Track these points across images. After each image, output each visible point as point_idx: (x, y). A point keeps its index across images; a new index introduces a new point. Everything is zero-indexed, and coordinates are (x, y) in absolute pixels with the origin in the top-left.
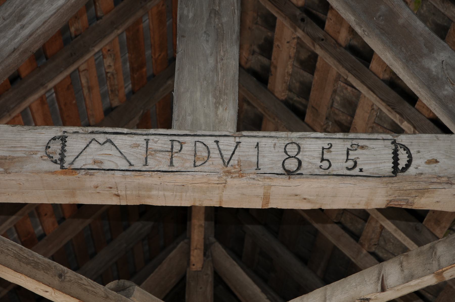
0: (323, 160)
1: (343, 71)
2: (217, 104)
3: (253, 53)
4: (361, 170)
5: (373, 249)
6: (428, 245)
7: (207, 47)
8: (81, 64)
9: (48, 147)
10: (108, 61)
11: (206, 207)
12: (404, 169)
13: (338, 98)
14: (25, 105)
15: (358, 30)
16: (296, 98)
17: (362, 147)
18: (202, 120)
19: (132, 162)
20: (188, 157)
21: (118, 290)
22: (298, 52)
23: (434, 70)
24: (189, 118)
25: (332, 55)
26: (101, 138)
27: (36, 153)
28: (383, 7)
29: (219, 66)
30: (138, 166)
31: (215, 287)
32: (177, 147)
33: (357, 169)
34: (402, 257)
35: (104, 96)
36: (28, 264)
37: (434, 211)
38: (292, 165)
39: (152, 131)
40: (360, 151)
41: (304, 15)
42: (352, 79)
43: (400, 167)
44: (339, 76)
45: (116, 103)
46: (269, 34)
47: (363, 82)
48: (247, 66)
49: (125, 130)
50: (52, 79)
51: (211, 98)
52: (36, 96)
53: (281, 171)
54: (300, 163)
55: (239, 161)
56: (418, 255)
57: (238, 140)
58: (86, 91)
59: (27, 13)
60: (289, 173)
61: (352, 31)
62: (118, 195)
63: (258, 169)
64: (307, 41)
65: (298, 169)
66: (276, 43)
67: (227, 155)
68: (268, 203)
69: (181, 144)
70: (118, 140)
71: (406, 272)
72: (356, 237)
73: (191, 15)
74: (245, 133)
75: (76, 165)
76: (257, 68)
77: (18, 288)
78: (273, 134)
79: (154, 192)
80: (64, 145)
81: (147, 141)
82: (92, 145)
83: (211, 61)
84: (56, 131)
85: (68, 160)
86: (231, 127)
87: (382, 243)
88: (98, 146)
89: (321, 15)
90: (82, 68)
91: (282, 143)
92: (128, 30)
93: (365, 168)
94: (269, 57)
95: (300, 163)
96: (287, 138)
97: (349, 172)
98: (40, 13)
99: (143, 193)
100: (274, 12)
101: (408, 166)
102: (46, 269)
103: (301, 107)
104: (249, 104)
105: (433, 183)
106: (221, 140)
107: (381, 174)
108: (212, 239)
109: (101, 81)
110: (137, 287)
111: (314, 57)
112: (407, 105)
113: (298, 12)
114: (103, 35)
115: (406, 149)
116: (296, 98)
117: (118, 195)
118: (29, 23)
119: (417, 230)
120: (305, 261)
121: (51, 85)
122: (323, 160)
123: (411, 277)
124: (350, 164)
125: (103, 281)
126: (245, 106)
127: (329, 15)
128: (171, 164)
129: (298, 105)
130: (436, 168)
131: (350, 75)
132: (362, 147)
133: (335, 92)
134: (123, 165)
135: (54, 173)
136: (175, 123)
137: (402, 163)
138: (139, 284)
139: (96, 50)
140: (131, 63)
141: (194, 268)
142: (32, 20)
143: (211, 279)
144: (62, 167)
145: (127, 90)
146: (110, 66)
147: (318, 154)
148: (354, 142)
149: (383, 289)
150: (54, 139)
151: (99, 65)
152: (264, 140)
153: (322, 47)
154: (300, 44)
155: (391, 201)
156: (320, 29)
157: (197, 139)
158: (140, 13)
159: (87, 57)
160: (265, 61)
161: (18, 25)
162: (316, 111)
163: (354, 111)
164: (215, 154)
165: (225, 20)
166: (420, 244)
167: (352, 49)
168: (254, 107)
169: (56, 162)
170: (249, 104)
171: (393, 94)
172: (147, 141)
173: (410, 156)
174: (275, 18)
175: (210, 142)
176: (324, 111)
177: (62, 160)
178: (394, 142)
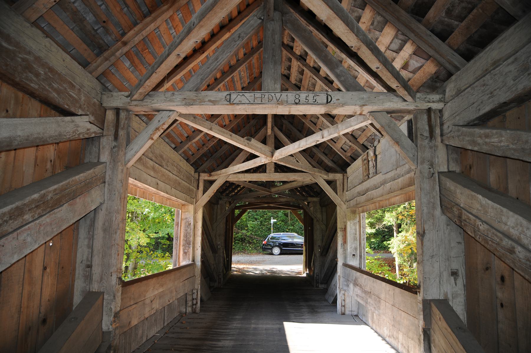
0: (306, 99)
1: (312, 75)
2: (275, 83)
3: (285, 69)
4: (317, 102)
5: (320, 128)
6: (336, 125)
7: (272, 66)
8: (234, 74)
9: (226, 97)
10: (242, 73)
11: (272, 114)
12: (330, 102)
13: (310, 83)
14: (219, 87)
15: (316, 61)
16: (298, 83)
17: (318, 95)
18: (270, 88)
19: (250, 101)
20: (266, 99)
21: (247, 139)
22: (298, 69)
23: (338, 72)
24: (267, 88)
25: (308, 70)
26: (241, 94)
27: (222, 99)
28: (324, 54)
29: (275, 72)
30: (252, 102)
31: (275, 140)
32: (263, 96)
33: (316, 102)
34: (328, 129)
35: (241, 84)
36: (222, 132)
37: (339, 115)
38: (297, 101)
39: (256, 92)
40: (317, 97)
41: (300, 58)
42: (314, 77)
43: (329, 101)
44: (310, 76)
45: (245, 86)
46: (290, 64)
47: (318, 78)
48: (283, 74)
49: (248, 92)
50: (226, 79)
51: (273, 81)
52: (222, 84)
53: (294, 103)
54: (299, 100)
55: (282, 100)
56: (333, 128)
57: (281, 94)
58: (236, 82)
59: (219, 58)
60: (296, 104)
61: (315, 62)
62: (246, 111)
63: (287, 102)
64: (301, 65)
65: (299, 102)
66: (292, 66)
67: (278, 98)
68: (290, 113)
69: (264, 95)
70: (246, 95)
71: (329, 133)
72: (315, 124)
73: (267, 57)
74: (283, 92)
75: (234, 102)
76: (286, 74)
77: (220, 140)
78: (292, 92)
79: (257, 110)
80: (230, 97)
81: (254, 95)
82: (238, 96)
83: (273, 70)
84: (228, 93)
85: (232, 101)
86: (279, 90)
87: (323, 126)
88: (240, 96)
89: (305, 58)
90: (235, 75)
91: (294, 94)
92: (248, 63)
93: (318, 102)
94: (290, 71)
95: (299, 100)
96: (296, 93)
97: (314, 103)
98: (222, 58)
99: (253, 110)
100: (291, 57)
101: (331, 101)
102: (227, 134)
103: (300, 86)
104: (284, 85)
105: (337, 106)
106: (276, 94)
107: (323, 103)
108: (274, 125)
109: (241, 79)
110: (252, 139)
111: (303, 70)
112: (330, 84)
113: (298, 57)
114: (241, 65)
115: (330, 96)
116: (298, 83)
117: (246, 111)
118: (219, 61)
119: (333, 122)
120: (300, 132)
121: (226, 80)
122: (306, 99)
123: (331, 134)
124: (314, 100)
125: (243, 137)
126: (283, 86)
127: (308, 57)
128: (262, 101)
129: (298, 85)
130: (339, 101)
131: (314, 76)
132: (318, 95)
133: (309, 81)
134: (248, 102)
135: (228, 105)
136: (262, 89)
137: (329, 100)
138: (253, 138)
139: (239, 69)
140: (249, 74)
141: (268, 134)
142: (220, 60)
143: (274, 137)
144: (230, 103)
145: (248, 82)
146: (243, 75)
147: (305, 98)
148: (315, 94)
149: (323, 138)
150: (227, 95)
151: (240, 74)
152: (289, 94)
153: (305, 67)
154: (299, 66)
155: (326, 112)
156: (305, 62)
157: (269, 94)
158: (251, 58)
159: (236, 72)
160: (289, 72)
161: (216, 62)
162: (304, 87)
163: (315, 87)
164: (274, 98)
165: (277, 58)
166: (332, 125)
167: (314, 68)
168: (285, 86)
169: (228, 102)
170: (284, 85)
171: (327, 81)
172: (254, 95)
173: (331, 98)
174: (292, 59)
175: (273, 94)
176: (306, 87)
177: (230, 101)
178: (327, 94)
